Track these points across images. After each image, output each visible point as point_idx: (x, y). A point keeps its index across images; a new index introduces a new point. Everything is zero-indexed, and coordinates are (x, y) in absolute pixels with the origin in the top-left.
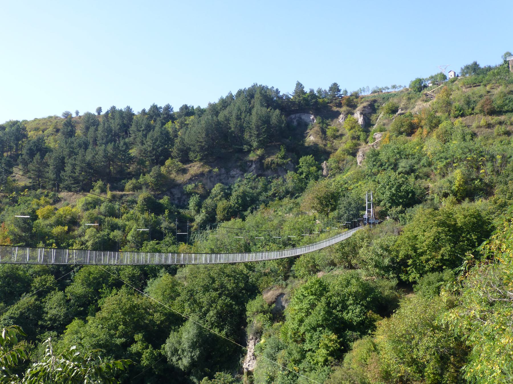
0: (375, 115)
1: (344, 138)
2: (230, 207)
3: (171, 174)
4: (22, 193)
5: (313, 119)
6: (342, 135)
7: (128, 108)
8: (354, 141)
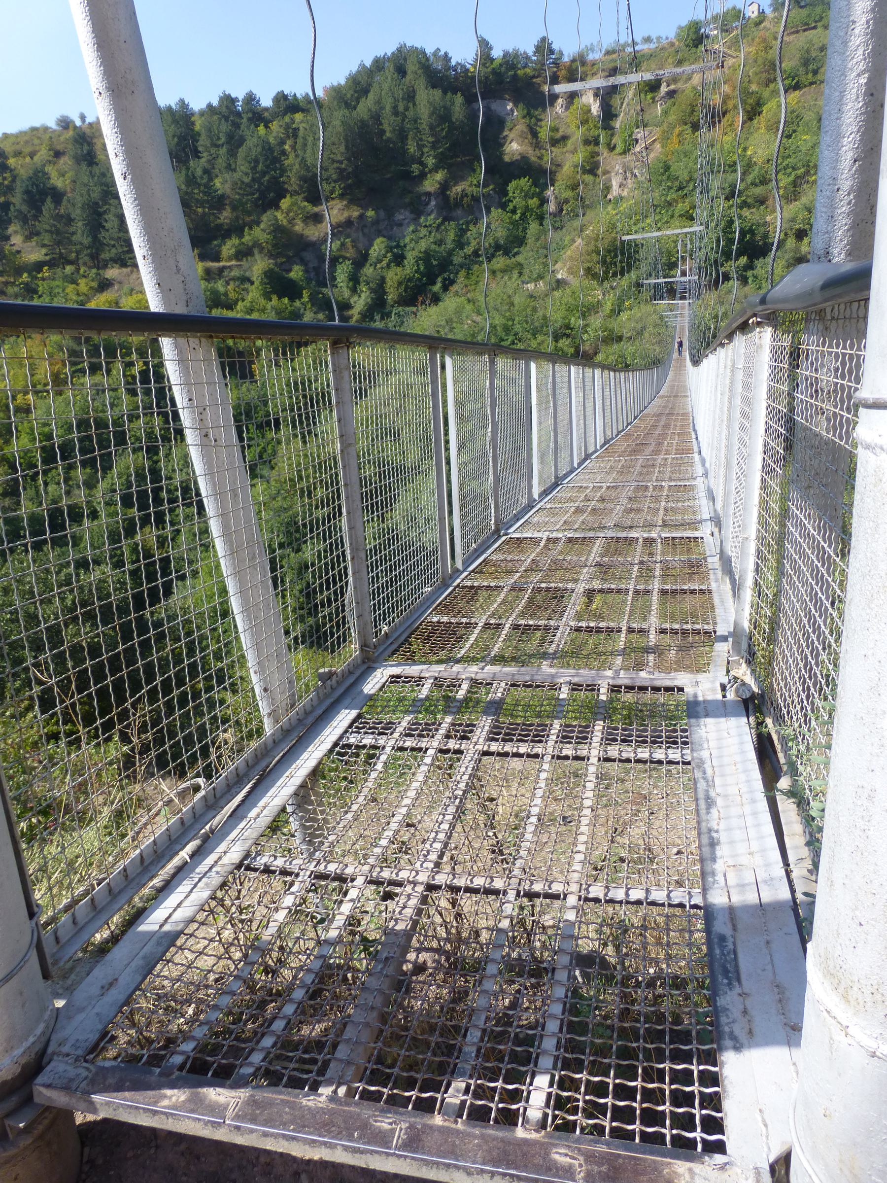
0: (618, 97)
1: (570, 144)
2: (410, 280)
3: (294, 225)
4: (40, 275)
5: (512, 110)
6: (565, 138)
7: (182, 101)
8: (589, 148)
